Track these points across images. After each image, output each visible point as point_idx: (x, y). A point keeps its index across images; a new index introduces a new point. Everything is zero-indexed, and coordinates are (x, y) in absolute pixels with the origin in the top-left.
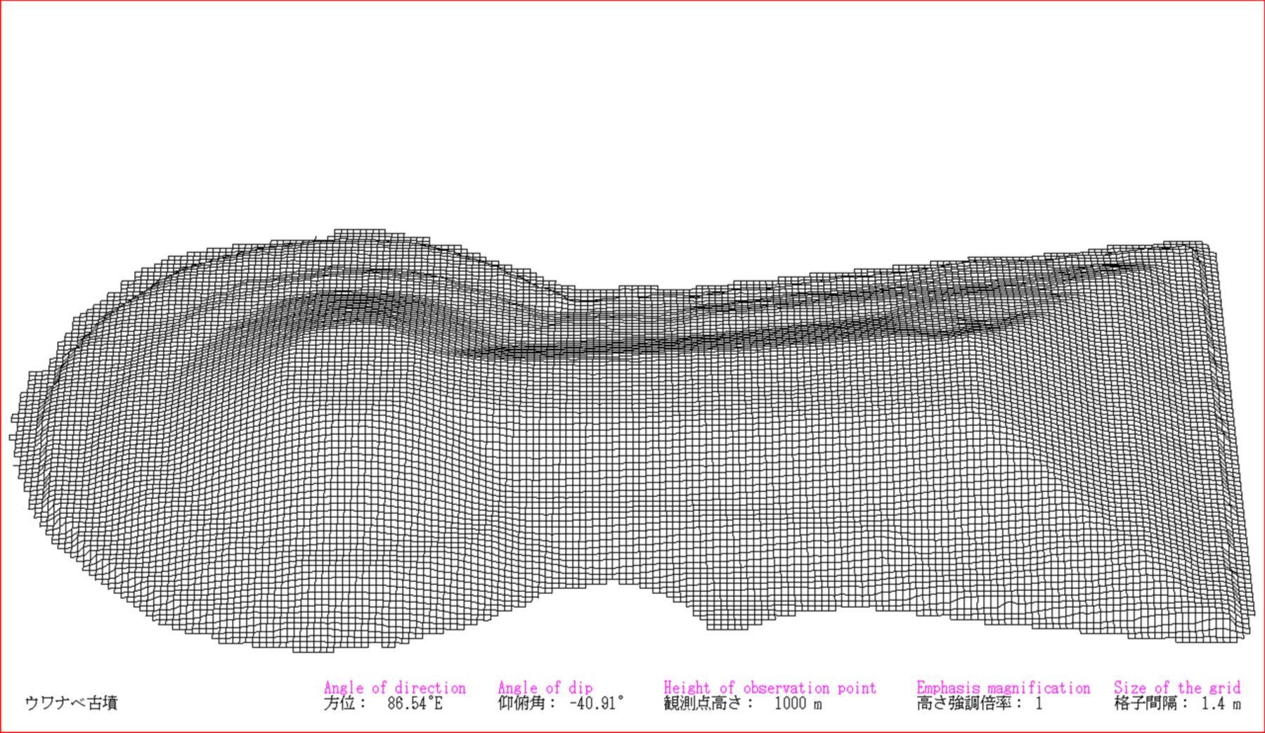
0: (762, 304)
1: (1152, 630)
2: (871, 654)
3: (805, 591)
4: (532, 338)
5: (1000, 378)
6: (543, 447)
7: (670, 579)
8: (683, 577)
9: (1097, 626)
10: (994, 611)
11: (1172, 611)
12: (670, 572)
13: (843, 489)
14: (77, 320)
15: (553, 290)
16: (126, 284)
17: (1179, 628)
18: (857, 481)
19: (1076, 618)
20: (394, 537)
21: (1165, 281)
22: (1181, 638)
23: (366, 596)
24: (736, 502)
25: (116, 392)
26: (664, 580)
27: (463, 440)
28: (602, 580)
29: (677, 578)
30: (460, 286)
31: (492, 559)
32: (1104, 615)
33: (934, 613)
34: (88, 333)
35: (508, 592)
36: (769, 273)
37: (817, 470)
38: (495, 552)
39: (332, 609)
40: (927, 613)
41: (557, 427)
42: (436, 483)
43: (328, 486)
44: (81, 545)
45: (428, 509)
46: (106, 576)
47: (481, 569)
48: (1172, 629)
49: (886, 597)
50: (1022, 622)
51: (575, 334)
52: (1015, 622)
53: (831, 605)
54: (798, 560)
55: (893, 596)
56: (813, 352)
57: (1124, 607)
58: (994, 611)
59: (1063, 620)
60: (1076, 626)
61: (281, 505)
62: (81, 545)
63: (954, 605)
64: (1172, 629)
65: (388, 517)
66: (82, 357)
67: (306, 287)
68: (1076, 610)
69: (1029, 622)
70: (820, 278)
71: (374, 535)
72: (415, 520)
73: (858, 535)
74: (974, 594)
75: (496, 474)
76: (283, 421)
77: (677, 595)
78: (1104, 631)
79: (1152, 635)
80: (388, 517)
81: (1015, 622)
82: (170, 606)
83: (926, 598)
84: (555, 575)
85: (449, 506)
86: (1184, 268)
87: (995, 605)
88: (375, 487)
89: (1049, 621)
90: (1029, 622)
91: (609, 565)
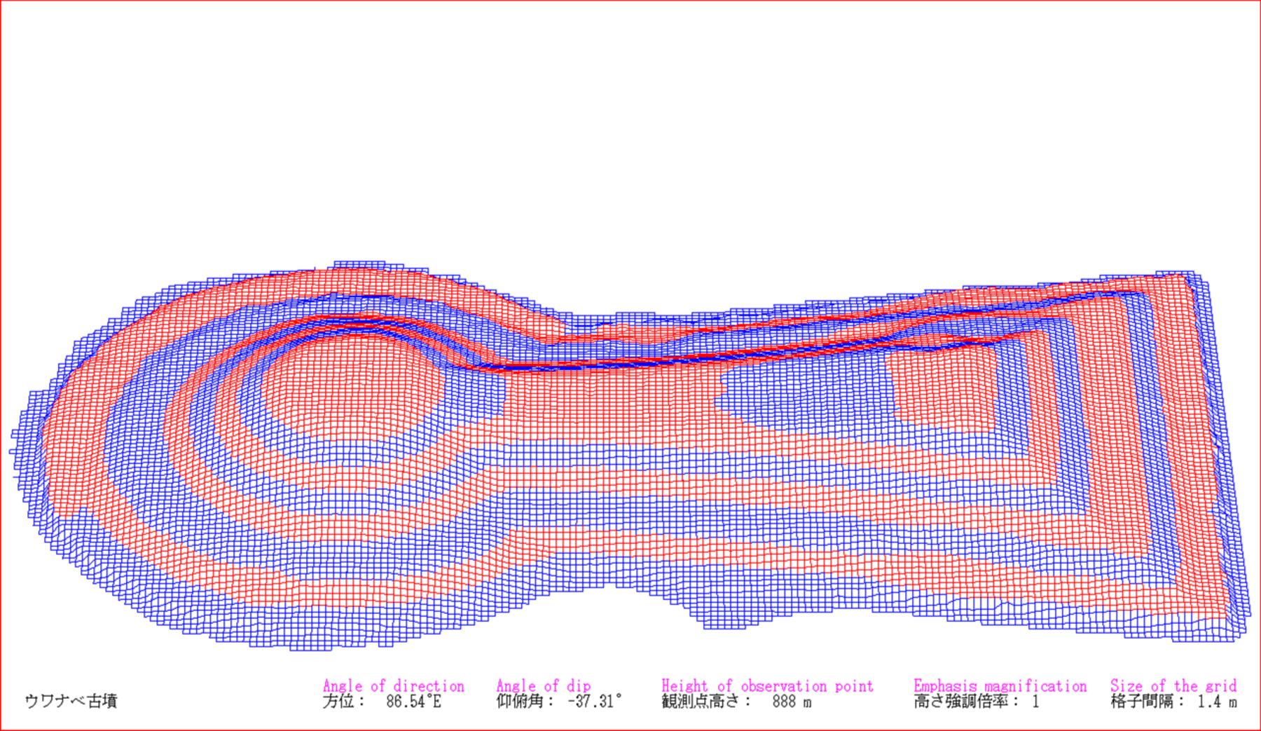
0: (759, 327)
1: (1155, 629)
2: (868, 654)
3: (593, 569)
4: (529, 357)
5: (1005, 395)
6: (554, 449)
7: (667, 582)
8: (680, 580)
9: (903, 604)
10: (991, 612)
11: (1161, 611)
12: (667, 576)
13: (806, 497)
14: (78, 345)
15: (550, 315)
16: (126, 311)
17: (1175, 627)
18: (880, 485)
19: (1073, 618)
20: (465, 555)
21: (1159, 312)
22: (1177, 638)
23: (367, 450)
24: (298, 545)
25: (117, 408)
26: (660, 583)
27: (441, 465)
28: (599, 581)
29: (674, 581)
30: (459, 311)
31: (485, 561)
32: (937, 597)
33: (964, 618)
34: (87, 355)
35: (505, 595)
36: (763, 299)
37: (839, 475)
38: (493, 555)
39: (359, 531)
40: (958, 618)
41: (534, 449)
42: (433, 489)
43: (319, 498)
44: (79, 551)
45: (426, 513)
46: (98, 576)
47: (479, 571)
48: (1169, 628)
49: (1045, 615)
50: (1019, 622)
51: (572, 354)
52: (855, 605)
53: (826, 607)
54: (794, 564)
55: (896, 597)
56: (820, 365)
57: (896, 589)
58: (991, 612)
59: (1059, 621)
60: (1073, 626)
61: (292, 521)
62: (79, 551)
63: (998, 611)
64: (1169, 628)
65: (474, 439)
66: (81, 378)
67: (307, 310)
68: (916, 594)
69: (869, 605)
70: (816, 305)
71: (444, 584)
72: (412, 517)
73: (787, 537)
74: (1161, 611)
75: (494, 482)
76: (281, 440)
77: (674, 596)
78: (1066, 626)
79: (1155, 635)
80: (474, 439)
81: (855, 605)
82: (155, 603)
83: (1093, 616)
84: (553, 579)
85: (433, 515)
86: (1178, 296)
87: (991, 606)
88: (373, 444)
89: (1100, 625)
90: (1026, 622)
91: (607, 567)
